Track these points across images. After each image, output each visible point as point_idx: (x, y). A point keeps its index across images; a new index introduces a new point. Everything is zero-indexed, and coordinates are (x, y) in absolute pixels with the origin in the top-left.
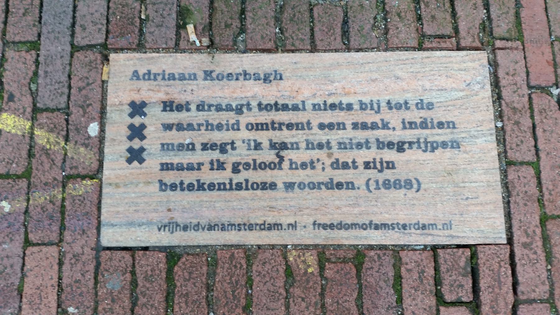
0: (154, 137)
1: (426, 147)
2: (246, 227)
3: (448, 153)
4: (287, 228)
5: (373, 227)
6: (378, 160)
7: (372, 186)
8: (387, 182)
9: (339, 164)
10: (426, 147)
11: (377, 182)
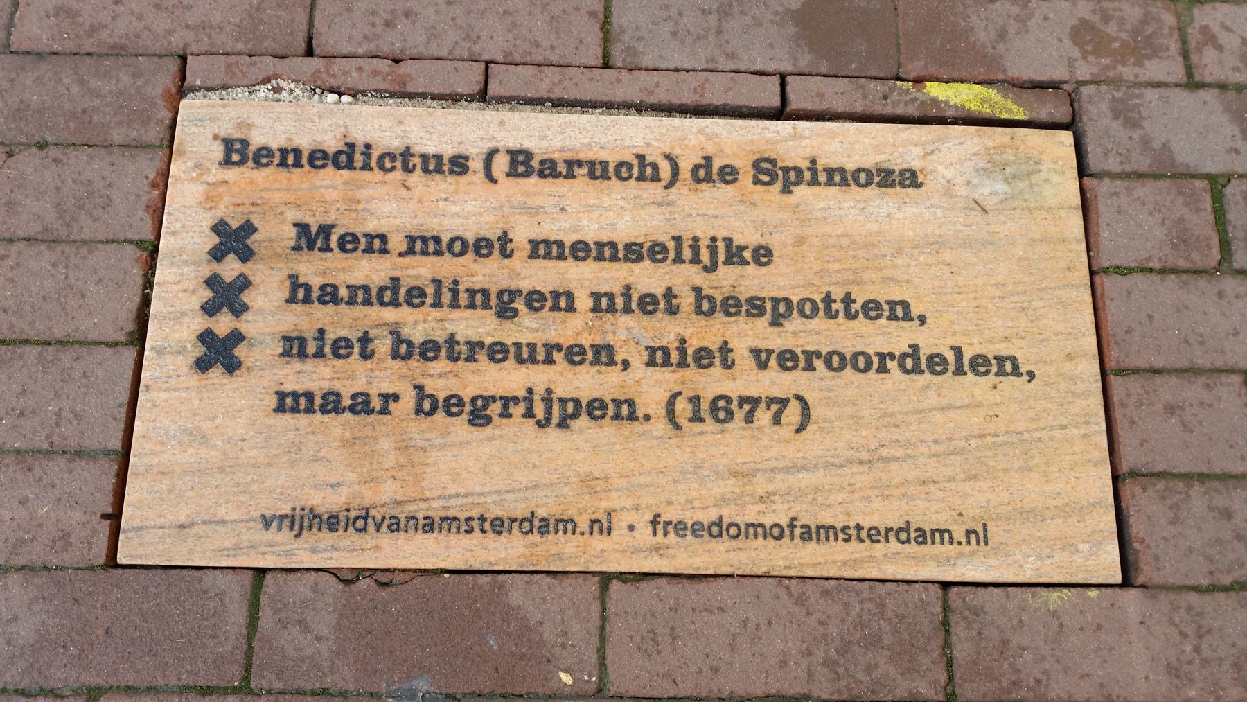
0: (267, 315)
1: (548, 411)
2: (487, 525)
3: (607, 431)
4: (964, 540)
5: (798, 531)
8: (722, 403)
9: (919, 359)
10: (548, 411)
11: (695, 400)
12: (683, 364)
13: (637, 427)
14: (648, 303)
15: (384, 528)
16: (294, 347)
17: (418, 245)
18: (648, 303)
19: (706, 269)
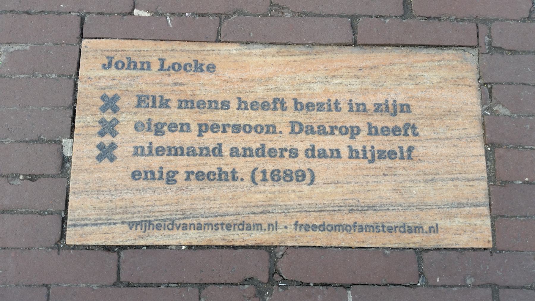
0: (127, 138)
4: (267, 228)
6: (390, 102)
7: (259, 177)
11: (264, 172)
12: (150, 153)
13: (237, 183)
14: (385, 131)
15: (180, 229)
16: (139, 152)
17: (184, 104)
18: (385, 131)
19: (392, 115)
